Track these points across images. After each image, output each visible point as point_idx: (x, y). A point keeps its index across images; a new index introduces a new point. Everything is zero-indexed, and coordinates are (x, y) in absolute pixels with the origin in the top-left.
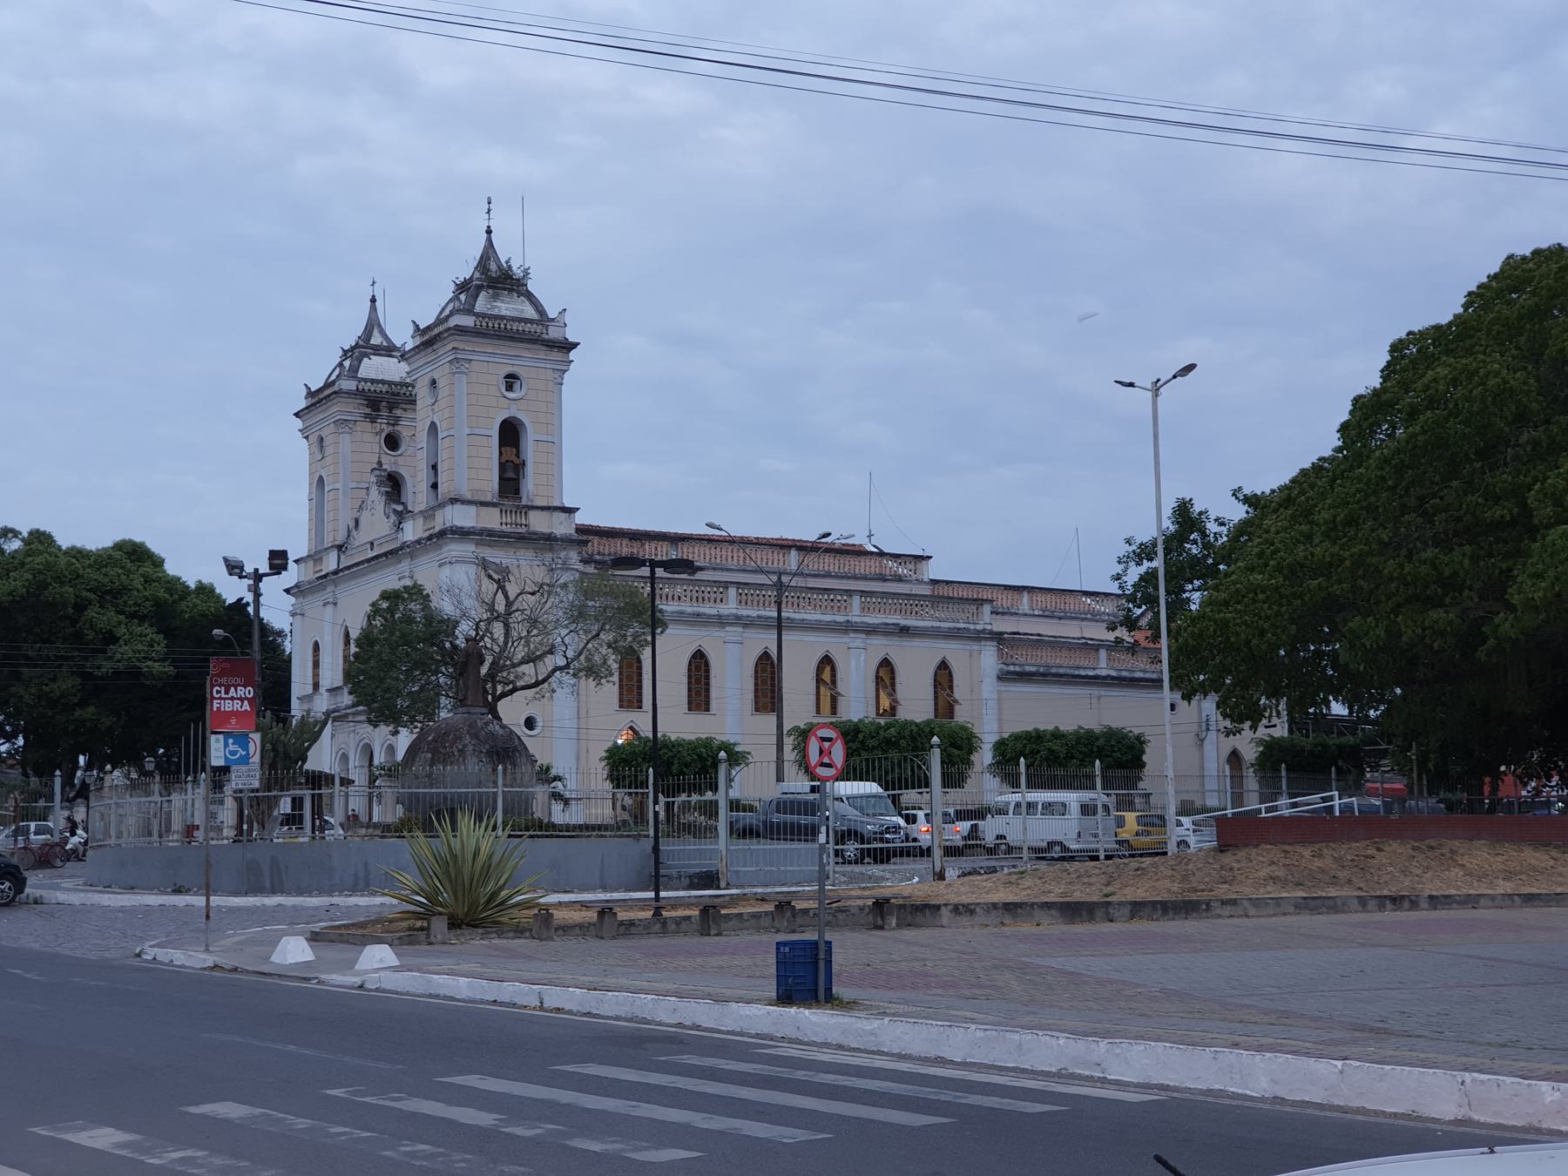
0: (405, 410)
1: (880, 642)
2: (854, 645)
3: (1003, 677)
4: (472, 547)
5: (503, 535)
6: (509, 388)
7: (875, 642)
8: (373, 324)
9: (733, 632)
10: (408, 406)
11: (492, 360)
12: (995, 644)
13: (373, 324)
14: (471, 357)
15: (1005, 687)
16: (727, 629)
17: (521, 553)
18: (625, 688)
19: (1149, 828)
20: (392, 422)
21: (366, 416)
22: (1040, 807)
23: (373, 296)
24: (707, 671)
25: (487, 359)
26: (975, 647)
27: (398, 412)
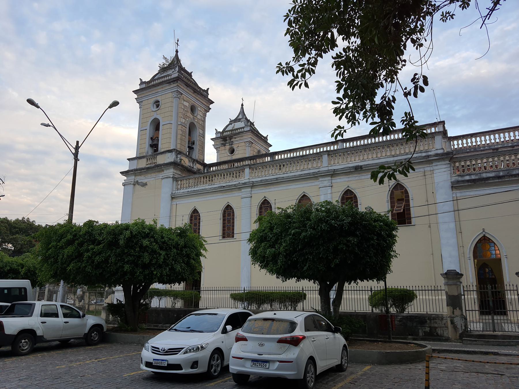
0: (235, 138)
1: (342, 180)
2: (321, 185)
3: (455, 186)
4: (133, 177)
5: (148, 169)
6: (158, 106)
7: (338, 180)
8: (242, 112)
9: (246, 192)
10: (236, 137)
11: (149, 98)
12: (448, 162)
13: (242, 112)
14: (142, 100)
15: (459, 194)
16: (242, 190)
17: (149, 176)
18: (197, 232)
19: (303, 296)
20: (231, 144)
21: (222, 144)
22: (481, 291)
23: (242, 104)
24: (234, 215)
25: (147, 98)
26: (428, 169)
27: (232, 140)
